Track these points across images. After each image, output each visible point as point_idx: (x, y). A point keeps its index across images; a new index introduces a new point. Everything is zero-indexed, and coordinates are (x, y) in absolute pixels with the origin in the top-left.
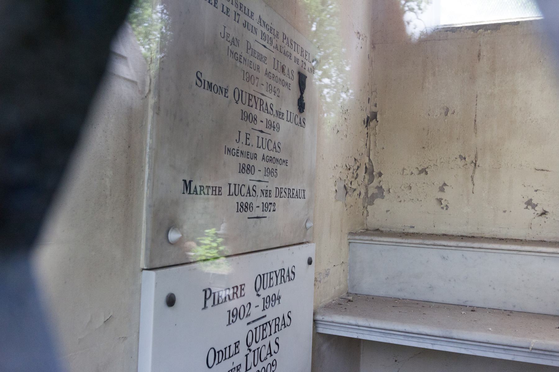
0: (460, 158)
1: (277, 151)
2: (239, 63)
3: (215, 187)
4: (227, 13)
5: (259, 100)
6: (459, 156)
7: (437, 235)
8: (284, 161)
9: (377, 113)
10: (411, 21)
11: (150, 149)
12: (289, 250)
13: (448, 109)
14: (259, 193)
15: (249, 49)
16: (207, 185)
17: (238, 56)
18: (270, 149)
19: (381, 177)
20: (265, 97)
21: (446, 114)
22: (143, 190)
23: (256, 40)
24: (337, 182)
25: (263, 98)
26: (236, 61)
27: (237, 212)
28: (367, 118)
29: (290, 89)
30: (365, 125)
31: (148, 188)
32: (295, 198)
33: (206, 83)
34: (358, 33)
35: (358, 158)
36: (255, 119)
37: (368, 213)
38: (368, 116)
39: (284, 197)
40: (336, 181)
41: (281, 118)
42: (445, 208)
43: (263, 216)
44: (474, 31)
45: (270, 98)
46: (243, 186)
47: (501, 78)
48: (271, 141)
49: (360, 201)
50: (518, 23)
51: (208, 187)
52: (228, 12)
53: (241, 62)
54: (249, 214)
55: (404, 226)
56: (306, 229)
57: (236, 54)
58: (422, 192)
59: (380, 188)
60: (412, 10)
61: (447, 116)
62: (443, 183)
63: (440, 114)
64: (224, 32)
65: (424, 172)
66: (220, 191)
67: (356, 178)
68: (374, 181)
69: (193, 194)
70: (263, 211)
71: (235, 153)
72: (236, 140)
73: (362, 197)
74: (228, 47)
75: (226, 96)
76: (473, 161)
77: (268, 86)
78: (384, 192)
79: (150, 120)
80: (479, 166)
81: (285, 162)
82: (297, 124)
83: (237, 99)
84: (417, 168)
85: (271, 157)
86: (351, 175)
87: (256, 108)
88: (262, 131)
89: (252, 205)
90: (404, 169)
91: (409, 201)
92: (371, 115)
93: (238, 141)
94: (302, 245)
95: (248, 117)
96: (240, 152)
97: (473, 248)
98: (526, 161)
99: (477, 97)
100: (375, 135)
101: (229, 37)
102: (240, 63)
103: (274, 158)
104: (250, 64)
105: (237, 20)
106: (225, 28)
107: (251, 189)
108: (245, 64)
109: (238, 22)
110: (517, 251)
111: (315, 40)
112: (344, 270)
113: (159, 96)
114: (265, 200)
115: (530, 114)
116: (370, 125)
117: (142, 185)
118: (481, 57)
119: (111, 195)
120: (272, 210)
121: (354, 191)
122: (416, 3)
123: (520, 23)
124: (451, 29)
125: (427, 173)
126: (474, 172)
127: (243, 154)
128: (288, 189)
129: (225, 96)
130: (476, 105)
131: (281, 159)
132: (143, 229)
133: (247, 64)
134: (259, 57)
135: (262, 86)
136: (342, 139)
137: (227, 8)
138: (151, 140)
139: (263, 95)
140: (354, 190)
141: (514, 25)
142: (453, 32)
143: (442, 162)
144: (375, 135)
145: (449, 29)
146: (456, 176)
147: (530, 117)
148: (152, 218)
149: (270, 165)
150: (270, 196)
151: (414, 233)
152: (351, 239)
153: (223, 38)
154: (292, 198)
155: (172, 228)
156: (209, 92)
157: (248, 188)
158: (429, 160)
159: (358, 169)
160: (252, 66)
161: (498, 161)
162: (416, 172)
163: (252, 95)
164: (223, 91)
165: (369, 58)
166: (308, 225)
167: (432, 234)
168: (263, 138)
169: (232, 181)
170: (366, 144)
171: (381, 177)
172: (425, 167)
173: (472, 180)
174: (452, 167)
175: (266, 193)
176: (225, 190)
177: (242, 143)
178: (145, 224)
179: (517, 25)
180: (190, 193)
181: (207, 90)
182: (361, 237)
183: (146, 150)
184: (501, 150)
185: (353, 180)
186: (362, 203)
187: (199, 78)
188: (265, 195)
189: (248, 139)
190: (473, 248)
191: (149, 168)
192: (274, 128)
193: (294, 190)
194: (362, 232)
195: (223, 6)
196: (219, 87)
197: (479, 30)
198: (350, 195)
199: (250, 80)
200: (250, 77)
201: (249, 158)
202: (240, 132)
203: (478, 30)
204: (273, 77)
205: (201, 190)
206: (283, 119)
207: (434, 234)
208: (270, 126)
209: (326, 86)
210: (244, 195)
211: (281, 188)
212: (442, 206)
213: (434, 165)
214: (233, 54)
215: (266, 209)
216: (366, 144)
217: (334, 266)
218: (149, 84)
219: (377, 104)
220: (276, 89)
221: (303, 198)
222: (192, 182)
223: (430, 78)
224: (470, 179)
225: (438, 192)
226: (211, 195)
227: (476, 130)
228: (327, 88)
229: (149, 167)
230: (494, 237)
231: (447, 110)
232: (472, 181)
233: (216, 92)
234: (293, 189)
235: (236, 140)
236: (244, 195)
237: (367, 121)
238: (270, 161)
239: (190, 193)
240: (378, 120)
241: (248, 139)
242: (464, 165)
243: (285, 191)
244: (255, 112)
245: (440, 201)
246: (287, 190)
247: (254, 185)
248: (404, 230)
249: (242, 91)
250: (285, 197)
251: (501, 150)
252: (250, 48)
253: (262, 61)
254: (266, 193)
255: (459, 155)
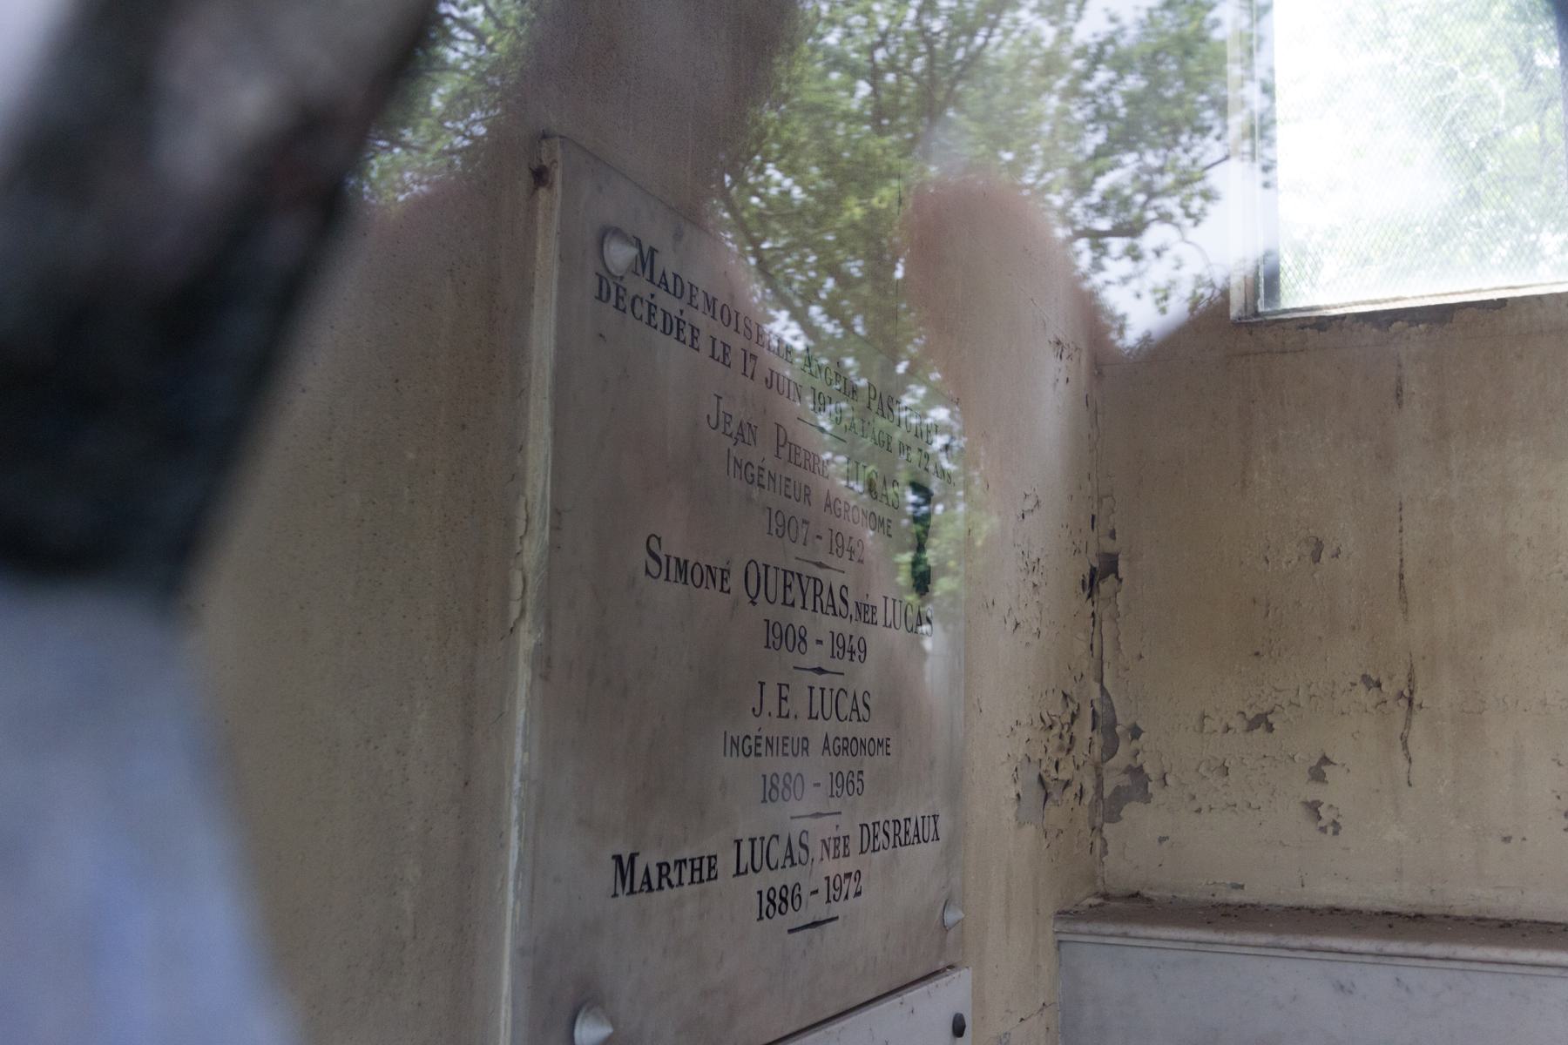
0: (1365, 683)
1: (861, 718)
2: (758, 488)
3: (698, 858)
4: (724, 359)
5: (812, 581)
6: (1359, 679)
7: (1313, 911)
8: (880, 744)
9: (1118, 555)
10: (1167, 249)
11: (522, 780)
12: (902, 1003)
13: (1321, 542)
14: (816, 850)
15: (783, 446)
16: (678, 859)
17: (755, 472)
18: (842, 718)
19: (1140, 739)
20: (825, 570)
21: (1316, 558)
22: (504, 903)
23: (798, 419)
24: (1018, 770)
25: (820, 573)
26: (750, 486)
27: (758, 920)
28: (1091, 570)
29: (890, 536)
30: (1087, 592)
31: (517, 896)
32: (913, 844)
33: (673, 563)
34: (1058, 343)
35: (1071, 688)
36: (803, 639)
37: (1106, 845)
38: (1091, 566)
39: (884, 847)
40: (1016, 770)
41: (868, 622)
42: (1330, 829)
43: (830, 917)
44: (1379, 326)
45: (840, 571)
46: (774, 839)
47: (1466, 456)
48: (846, 693)
49: (1083, 812)
50: (1502, 302)
51: (681, 863)
52: (725, 354)
53: (763, 487)
54: (793, 918)
55: (1215, 883)
56: (944, 928)
57: (749, 466)
58: (1261, 785)
59: (1137, 772)
60: (1165, 218)
61: (1317, 564)
62: (1320, 756)
63: (1299, 559)
64: (718, 411)
65: (1263, 725)
66: (714, 867)
67: (1069, 750)
68: (1118, 752)
69: (641, 890)
70: (829, 901)
71: (750, 747)
72: (754, 710)
73: (1087, 800)
74: (729, 450)
75: (726, 588)
76: (1402, 692)
77: (834, 537)
78: (1149, 783)
79: (524, 697)
80: (1420, 706)
81: (883, 744)
82: (912, 630)
83: (753, 591)
84: (1243, 713)
85: (846, 739)
86: (1056, 742)
87: (804, 607)
88: (820, 671)
89: (800, 889)
90: (1203, 717)
91: (1223, 809)
92: (1100, 563)
93: (757, 712)
94: (937, 982)
95: (783, 637)
96: (763, 742)
97: (1427, 958)
98: (1557, 691)
99: (1401, 509)
100: (1115, 618)
101: (729, 423)
102: (760, 490)
103: (855, 738)
104: (787, 486)
105: (749, 373)
106: (720, 401)
107: (795, 843)
108: (772, 489)
109: (752, 377)
110: (1561, 967)
111: (904, 306)
112: (1048, 1028)
113: (549, 626)
114: (832, 867)
115: (1558, 556)
116: (1099, 592)
117: (501, 889)
118: (1404, 398)
119: (415, 937)
120: (851, 895)
121: (1065, 788)
122: (1177, 199)
123: (1508, 304)
124: (1314, 321)
125: (1270, 728)
126: (1408, 723)
127: (771, 747)
128: (894, 821)
129: (722, 590)
130: (1401, 531)
131: (872, 739)
132: (502, 1022)
133: (778, 490)
134: (807, 462)
135: (818, 540)
136: (1027, 644)
137: (725, 345)
138: (527, 754)
139: (820, 565)
140: (1063, 784)
141: (1491, 310)
142: (1319, 330)
143: (1314, 696)
144: (1115, 618)
145: (1308, 323)
146: (1357, 736)
147: (1560, 565)
148: (529, 988)
149: (846, 763)
150: (847, 853)
151: (1245, 905)
152: (1064, 933)
153: (714, 429)
154: (905, 844)
155: (584, 1009)
156: (680, 587)
157: (786, 843)
158: (1276, 690)
159: (1072, 722)
160: (790, 492)
161: (1476, 692)
162: (1237, 724)
163: (792, 573)
164: (716, 576)
165: (1087, 405)
166: (951, 917)
167: (1299, 909)
168: (823, 690)
169: (744, 833)
170: (1092, 645)
171: (1138, 739)
172: (1265, 711)
173: (1405, 747)
174: (1344, 710)
175: (836, 847)
176: (726, 864)
177: (770, 714)
178: (509, 1008)
179: (1499, 308)
180: (632, 892)
181: (676, 581)
182: (1094, 927)
183: (511, 784)
184: (1481, 658)
185: (1062, 755)
186: (1089, 818)
187: (654, 553)
188: (832, 855)
189: (786, 699)
190: (1427, 958)
191: (520, 838)
192: (852, 652)
193: (908, 822)
194: (1095, 906)
195: (714, 340)
196: (705, 569)
197: (1394, 325)
198: (1056, 804)
199: (786, 533)
200: (787, 521)
201: (787, 755)
202: (762, 684)
203: (1390, 323)
204: (846, 511)
205: (661, 876)
206: (874, 622)
207: (1303, 907)
208: (841, 652)
209: (937, 428)
210: (776, 867)
211: (874, 824)
212: (1322, 823)
213: (1291, 703)
214: (740, 467)
215: (837, 894)
216: (1092, 645)
217: (1022, 1019)
218: (520, 594)
219: (1117, 531)
220: (853, 544)
221: (933, 840)
222: (637, 858)
223: (1264, 457)
224: (1399, 743)
225: (1307, 783)
226: (689, 884)
227: (1407, 602)
228: (942, 433)
229: (520, 831)
230: (1481, 915)
231: (1319, 546)
232: (1403, 749)
233: (698, 583)
234: (905, 820)
235: (754, 710)
236: (776, 867)
237: (1092, 581)
238: (845, 752)
239: (632, 892)
240: (1120, 576)
241: (786, 699)
242: (1378, 704)
243: (886, 830)
244: (800, 618)
245: (1313, 807)
246: (892, 824)
247: (804, 831)
248: (1213, 895)
249: (767, 567)
250: (886, 846)
251: (1481, 658)
252: (785, 443)
253: (816, 471)
254: (836, 847)
255: (1361, 674)
